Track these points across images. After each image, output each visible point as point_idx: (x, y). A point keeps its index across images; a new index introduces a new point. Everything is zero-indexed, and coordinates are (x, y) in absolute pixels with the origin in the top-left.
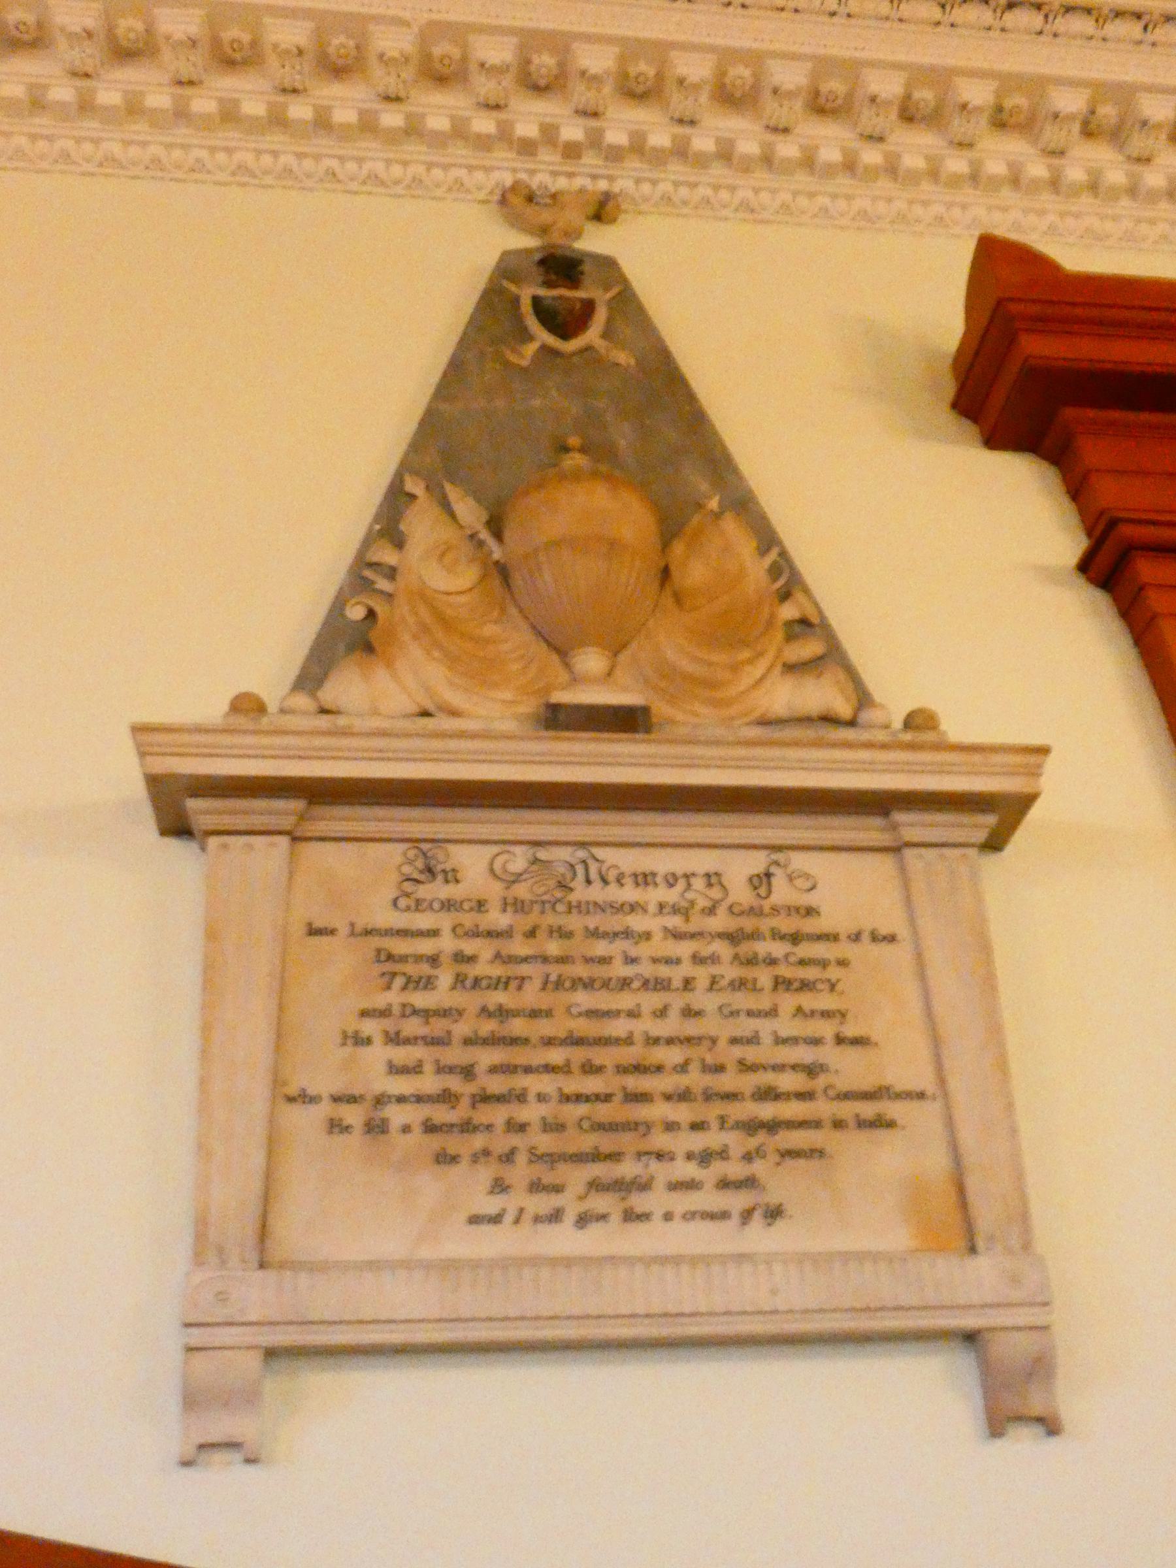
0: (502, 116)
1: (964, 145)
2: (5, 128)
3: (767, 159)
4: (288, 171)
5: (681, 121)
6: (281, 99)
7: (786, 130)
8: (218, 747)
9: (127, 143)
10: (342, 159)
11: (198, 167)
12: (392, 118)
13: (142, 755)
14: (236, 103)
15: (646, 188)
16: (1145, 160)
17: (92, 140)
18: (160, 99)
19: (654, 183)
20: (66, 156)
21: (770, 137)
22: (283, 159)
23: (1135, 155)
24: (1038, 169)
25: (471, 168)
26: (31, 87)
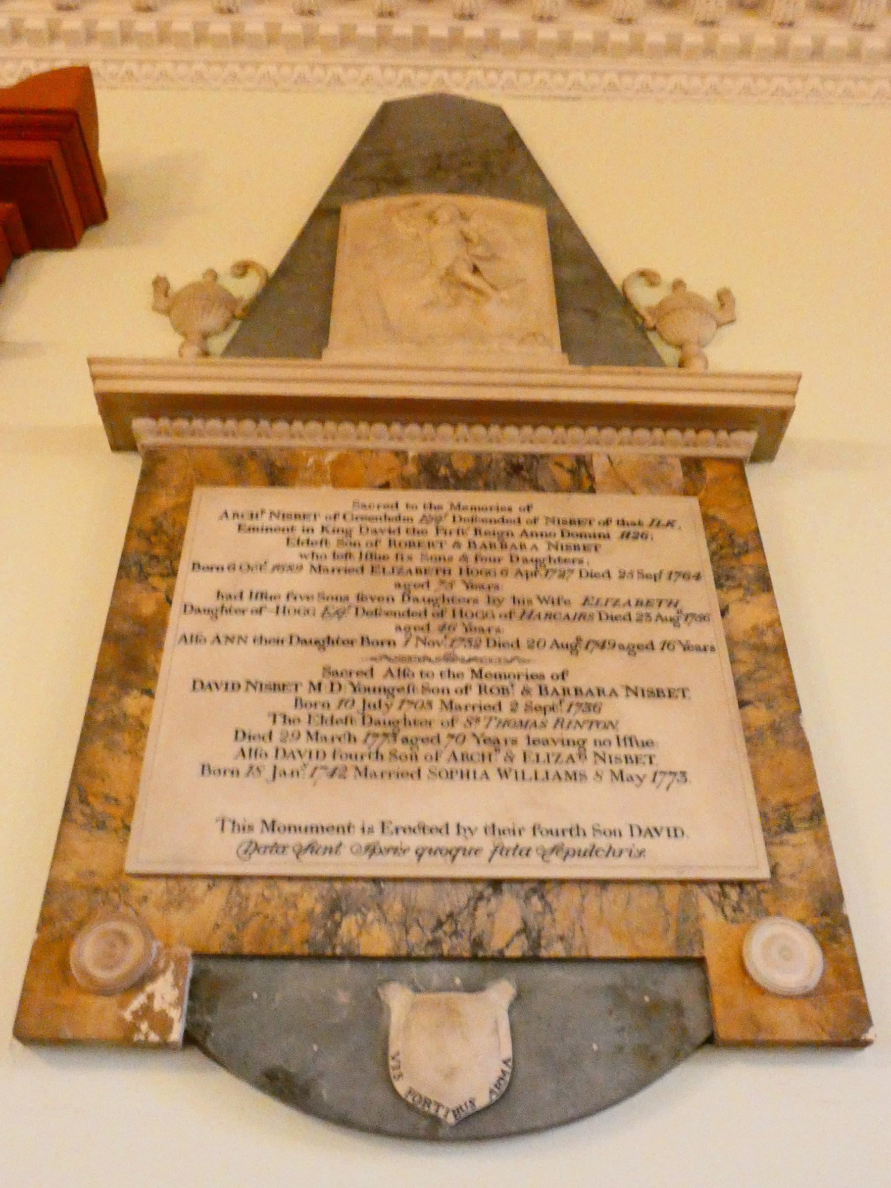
0: (234, 18)
1: (625, 21)
2: (2, 55)
3: (854, 53)
4: (200, 76)
5: (782, 24)
6: (859, 33)
7: (471, 16)
8: (491, 370)
9: (587, 73)
10: (654, 74)
11: (302, 79)
12: (547, 33)
13: (94, 378)
14: (425, 29)
15: (286, 70)
16: (867, 27)
17: (392, 66)
18: (368, 28)
19: (293, 65)
20: (337, 80)
21: (457, 23)
22: (298, 69)
23: (860, 22)
24: (694, 37)
25: (856, 80)
26: (269, 25)
